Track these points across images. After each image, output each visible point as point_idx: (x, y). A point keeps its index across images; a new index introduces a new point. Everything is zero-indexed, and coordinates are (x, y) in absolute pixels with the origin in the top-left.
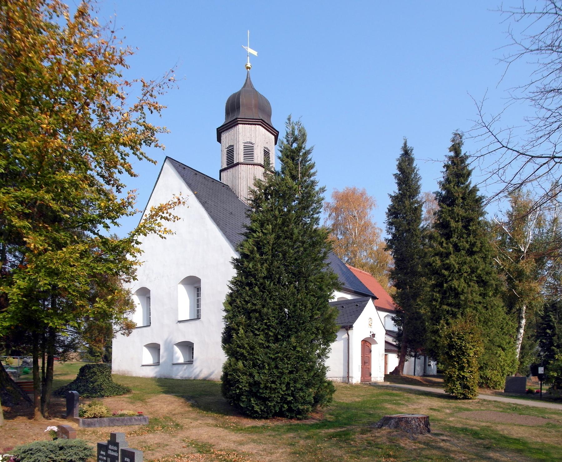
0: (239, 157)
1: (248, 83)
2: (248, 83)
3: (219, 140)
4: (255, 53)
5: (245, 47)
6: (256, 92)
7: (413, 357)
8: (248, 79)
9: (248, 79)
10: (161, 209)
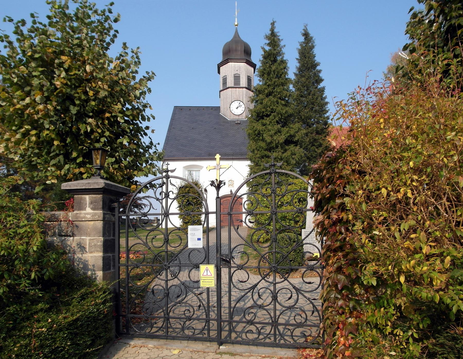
0: (230, 82)
1: (237, 35)
2: (237, 35)
3: (219, 72)
6: (242, 41)
7: (261, 276)
8: (237, 33)
9: (237, 33)
10: (148, 197)
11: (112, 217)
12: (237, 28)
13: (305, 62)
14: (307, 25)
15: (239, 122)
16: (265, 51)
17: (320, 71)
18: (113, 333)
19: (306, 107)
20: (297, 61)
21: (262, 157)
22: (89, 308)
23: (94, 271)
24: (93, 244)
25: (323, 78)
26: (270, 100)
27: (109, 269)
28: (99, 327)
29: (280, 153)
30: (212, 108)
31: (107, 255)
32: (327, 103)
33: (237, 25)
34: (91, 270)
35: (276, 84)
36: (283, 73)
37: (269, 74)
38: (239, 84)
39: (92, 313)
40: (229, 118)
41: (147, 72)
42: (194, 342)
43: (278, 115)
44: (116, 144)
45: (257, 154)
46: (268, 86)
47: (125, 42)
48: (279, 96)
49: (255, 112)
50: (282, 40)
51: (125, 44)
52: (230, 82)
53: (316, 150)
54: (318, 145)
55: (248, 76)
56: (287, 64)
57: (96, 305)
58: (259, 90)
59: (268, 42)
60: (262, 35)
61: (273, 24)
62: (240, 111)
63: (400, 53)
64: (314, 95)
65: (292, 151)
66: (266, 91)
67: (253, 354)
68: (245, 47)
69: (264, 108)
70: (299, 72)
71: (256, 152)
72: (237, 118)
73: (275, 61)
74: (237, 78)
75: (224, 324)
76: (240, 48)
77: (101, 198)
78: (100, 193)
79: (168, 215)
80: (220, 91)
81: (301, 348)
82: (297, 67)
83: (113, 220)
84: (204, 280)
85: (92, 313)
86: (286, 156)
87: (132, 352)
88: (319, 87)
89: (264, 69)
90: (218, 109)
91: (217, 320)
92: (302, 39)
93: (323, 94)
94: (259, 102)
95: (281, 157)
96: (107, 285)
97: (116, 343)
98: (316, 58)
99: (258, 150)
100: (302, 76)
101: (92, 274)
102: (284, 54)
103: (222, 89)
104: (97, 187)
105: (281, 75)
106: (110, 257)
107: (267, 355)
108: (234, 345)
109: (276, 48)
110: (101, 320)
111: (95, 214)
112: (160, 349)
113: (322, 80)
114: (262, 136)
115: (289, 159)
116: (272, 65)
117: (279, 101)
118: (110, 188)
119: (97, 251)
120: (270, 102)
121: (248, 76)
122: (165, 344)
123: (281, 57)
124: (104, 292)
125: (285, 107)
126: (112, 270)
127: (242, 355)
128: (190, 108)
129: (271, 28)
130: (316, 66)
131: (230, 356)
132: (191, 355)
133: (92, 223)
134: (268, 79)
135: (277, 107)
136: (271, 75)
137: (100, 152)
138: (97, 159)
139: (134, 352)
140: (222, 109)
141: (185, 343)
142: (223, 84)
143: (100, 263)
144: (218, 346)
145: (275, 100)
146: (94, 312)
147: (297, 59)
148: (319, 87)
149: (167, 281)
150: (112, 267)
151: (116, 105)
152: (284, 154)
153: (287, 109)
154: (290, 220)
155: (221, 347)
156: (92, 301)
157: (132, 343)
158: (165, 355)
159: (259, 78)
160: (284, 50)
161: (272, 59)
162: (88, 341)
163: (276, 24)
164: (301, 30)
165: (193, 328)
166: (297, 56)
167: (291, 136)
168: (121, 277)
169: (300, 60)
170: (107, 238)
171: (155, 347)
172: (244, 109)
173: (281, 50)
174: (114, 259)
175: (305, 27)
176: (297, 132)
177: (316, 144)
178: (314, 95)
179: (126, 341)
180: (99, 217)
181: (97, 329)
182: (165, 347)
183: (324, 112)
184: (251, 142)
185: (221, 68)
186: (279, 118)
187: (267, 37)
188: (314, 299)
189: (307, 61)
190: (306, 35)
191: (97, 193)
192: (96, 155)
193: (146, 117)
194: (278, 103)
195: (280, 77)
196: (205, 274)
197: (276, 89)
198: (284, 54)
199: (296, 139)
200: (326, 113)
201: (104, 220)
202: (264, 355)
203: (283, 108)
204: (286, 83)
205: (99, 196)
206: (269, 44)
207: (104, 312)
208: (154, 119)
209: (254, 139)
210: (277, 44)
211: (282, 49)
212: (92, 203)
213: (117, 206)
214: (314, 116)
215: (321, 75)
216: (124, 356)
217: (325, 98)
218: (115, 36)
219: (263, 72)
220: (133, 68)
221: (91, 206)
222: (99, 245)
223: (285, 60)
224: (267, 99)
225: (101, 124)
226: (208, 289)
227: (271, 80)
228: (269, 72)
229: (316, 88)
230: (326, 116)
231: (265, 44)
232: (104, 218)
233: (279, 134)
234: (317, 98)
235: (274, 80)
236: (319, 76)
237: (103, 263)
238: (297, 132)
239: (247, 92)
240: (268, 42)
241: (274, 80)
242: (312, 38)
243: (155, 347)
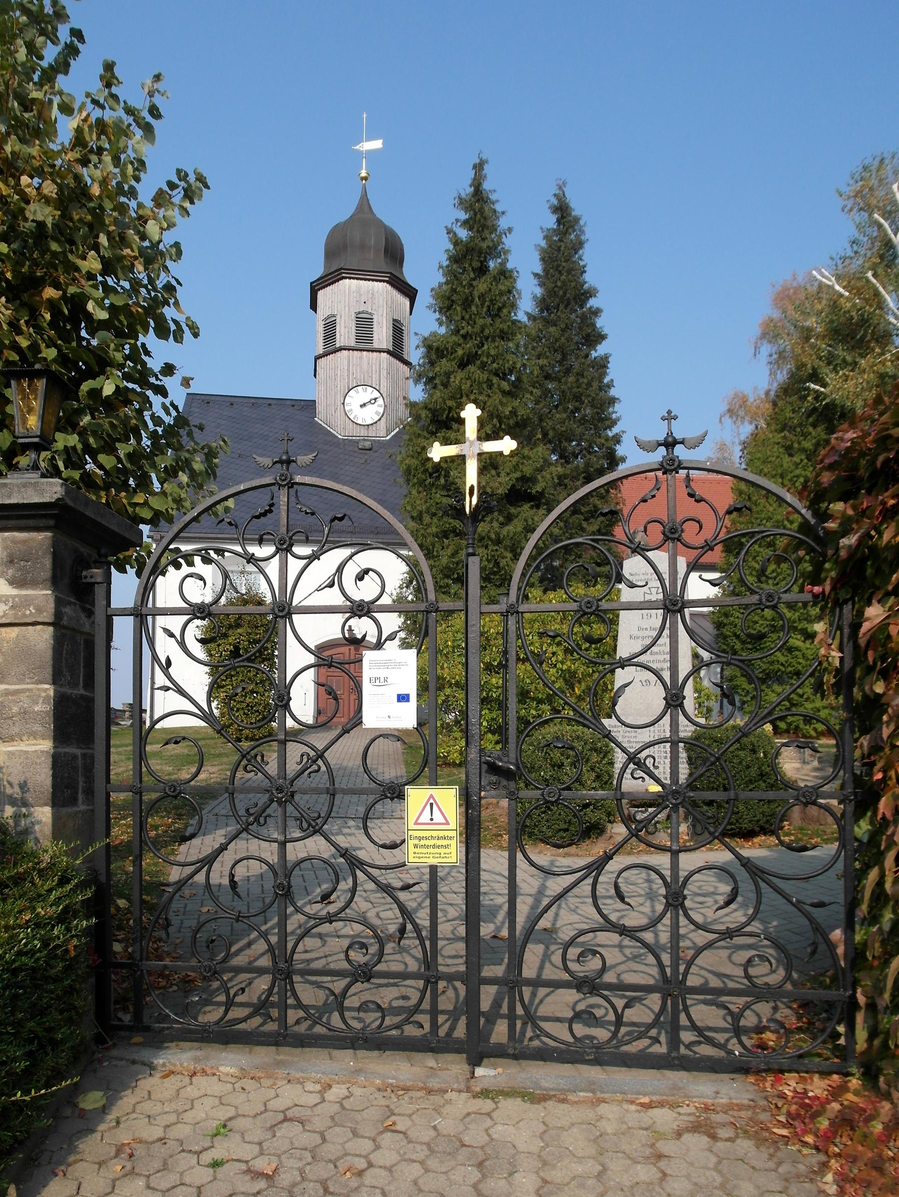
0: (345, 334)
1: (364, 204)
2: (364, 204)
3: (314, 306)
4: (377, 144)
5: (357, 147)
8: (364, 198)
9: (364, 198)
11: (83, 616)
12: (364, 186)
13: (559, 284)
14: (564, 183)
15: (368, 444)
16: (456, 242)
17: (597, 312)
18: (88, 1030)
19: (557, 407)
20: (536, 282)
21: (445, 535)
22: (11, 937)
23: (25, 804)
24: (15, 709)
25: (605, 331)
26: (469, 378)
27: (73, 801)
28: (49, 1006)
29: (495, 524)
30: (294, 403)
31: (66, 750)
32: (613, 401)
33: (366, 179)
34: (13, 802)
35: (487, 332)
36: (504, 306)
37: (467, 303)
38: (371, 341)
39: (26, 954)
40: (340, 431)
41: (179, 171)
42: (376, 1053)
43: (492, 419)
44: (78, 401)
45: (429, 525)
46: (464, 337)
47: (110, 58)
48: (495, 365)
49: (426, 407)
50: (503, 213)
51: (109, 67)
52: (345, 334)
53: (585, 524)
54: (590, 512)
55: (394, 320)
56: (515, 281)
57: (38, 925)
58: (438, 349)
59: (463, 216)
60: (450, 200)
61: (479, 167)
62: (369, 415)
63: (814, 272)
64: (580, 374)
65: (526, 520)
66: (460, 352)
67: (606, 1096)
68: (387, 239)
69: (452, 398)
70: (542, 311)
71: (427, 519)
72: (363, 432)
73: (482, 270)
74: (364, 324)
75: (534, 995)
76: (375, 240)
77: (48, 543)
78: (42, 523)
79: (289, 615)
80: (317, 358)
81: (768, 1070)
82: (535, 297)
83: (87, 628)
84: (420, 839)
85: (26, 954)
86: (511, 535)
87: (167, 1095)
88: (594, 354)
89: (454, 291)
90: (310, 406)
91: (464, 978)
92: (551, 221)
93: (604, 374)
94: (437, 381)
95: (497, 534)
96: (73, 853)
97: (100, 1061)
98: (587, 277)
99: (434, 514)
100: (548, 322)
101: (17, 817)
102: (507, 252)
103: (321, 351)
104: (36, 500)
105: (500, 309)
106: (75, 757)
107: (654, 1098)
108: (524, 1063)
109: (486, 233)
110: (56, 980)
111: (26, 602)
112: (267, 1082)
113: (602, 337)
114: (447, 475)
115: (519, 542)
116: (474, 279)
117: (495, 380)
118: (81, 509)
119: (33, 735)
120: (469, 383)
121: (394, 320)
122: (279, 1064)
123: (499, 261)
124: (64, 881)
125: (510, 399)
126: (82, 807)
127: (564, 1101)
128: (231, 401)
129: (475, 179)
130: (588, 299)
131: (528, 1105)
132: (384, 1102)
133: (13, 632)
134: (463, 318)
135: (489, 396)
136: (474, 308)
137: (41, 384)
138: (30, 410)
139: (173, 1093)
140: (320, 408)
141: (346, 1059)
142: (326, 338)
143: (43, 777)
144: (467, 1067)
145: (484, 376)
146: (32, 952)
147: (536, 275)
148: (594, 354)
149: (283, 845)
150: (81, 797)
151: (84, 258)
152: (506, 528)
153: (516, 403)
154: (540, 701)
155: (480, 1071)
156: (20, 912)
157: (160, 1060)
158: (289, 1103)
159: (437, 315)
160: (508, 242)
161: (476, 264)
162: (15, 1060)
163: (487, 169)
164: (548, 196)
165: (379, 1006)
166: (538, 268)
167: (524, 479)
168: (115, 831)
169: (544, 279)
170: (68, 691)
171: (244, 1074)
172: (381, 410)
173: (500, 242)
174: (89, 769)
175: (560, 188)
176: (540, 470)
177: (583, 509)
178: (580, 374)
179: (145, 1054)
180: (39, 610)
181: (43, 1012)
182: (281, 1072)
183: (607, 423)
184: (414, 492)
185: (321, 294)
186: (495, 426)
187: (462, 203)
188: (821, 905)
189: (564, 282)
190: (562, 210)
191: (31, 522)
192: (25, 398)
193: (173, 327)
194: (490, 387)
195: (497, 315)
196: (425, 817)
197: (486, 347)
198: (507, 252)
199: (538, 488)
200: (610, 427)
201: (56, 624)
202: (645, 1100)
203: (504, 400)
204: (514, 334)
205: (42, 538)
206: (466, 223)
207: (67, 951)
208: (196, 335)
209: (421, 483)
210: (489, 223)
211: (504, 239)
212: (11, 562)
213: (99, 580)
214: (578, 431)
215: (600, 323)
216: (139, 1107)
217: (610, 386)
218: (71, 51)
219: (449, 298)
220: (136, 140)
221: (10, 572)
222: (38, 713)
223: (511, 271)
224: (460, 374)
225: (27, 322)
226: (433, 869)
227: (472, 322)
228: (467, 299)
229: (587, 356)
230: (610, 434)
231: (457, 220)
232: (58, 614)
233: (493, 472)
234: (589, 384)
235: (480, 322)
236: (593, 325)
237: (54, 776)
238: (540, 470)
239: (390, 364)
240: (463, 216)
241: (480, 322)
242: (577, 220)
243: (244, 1074)
